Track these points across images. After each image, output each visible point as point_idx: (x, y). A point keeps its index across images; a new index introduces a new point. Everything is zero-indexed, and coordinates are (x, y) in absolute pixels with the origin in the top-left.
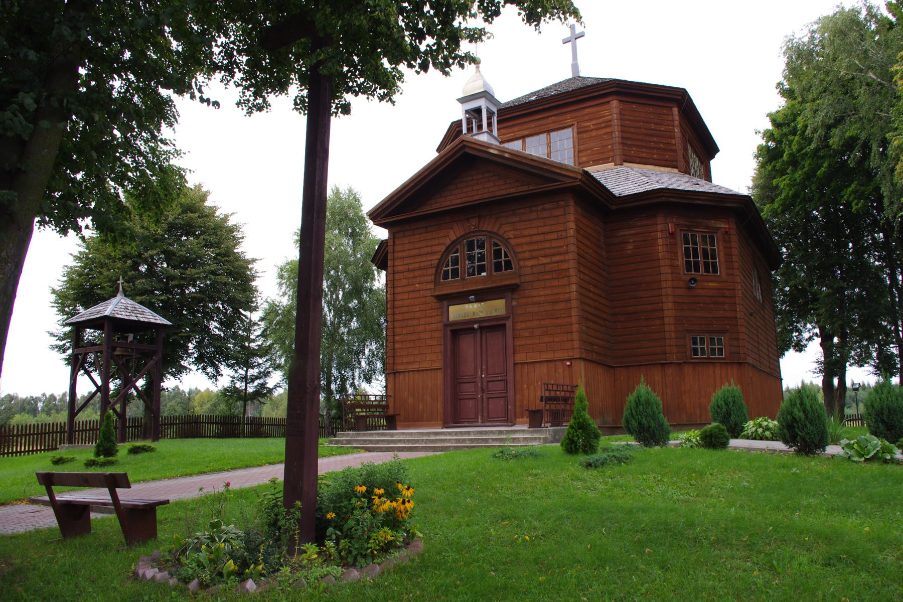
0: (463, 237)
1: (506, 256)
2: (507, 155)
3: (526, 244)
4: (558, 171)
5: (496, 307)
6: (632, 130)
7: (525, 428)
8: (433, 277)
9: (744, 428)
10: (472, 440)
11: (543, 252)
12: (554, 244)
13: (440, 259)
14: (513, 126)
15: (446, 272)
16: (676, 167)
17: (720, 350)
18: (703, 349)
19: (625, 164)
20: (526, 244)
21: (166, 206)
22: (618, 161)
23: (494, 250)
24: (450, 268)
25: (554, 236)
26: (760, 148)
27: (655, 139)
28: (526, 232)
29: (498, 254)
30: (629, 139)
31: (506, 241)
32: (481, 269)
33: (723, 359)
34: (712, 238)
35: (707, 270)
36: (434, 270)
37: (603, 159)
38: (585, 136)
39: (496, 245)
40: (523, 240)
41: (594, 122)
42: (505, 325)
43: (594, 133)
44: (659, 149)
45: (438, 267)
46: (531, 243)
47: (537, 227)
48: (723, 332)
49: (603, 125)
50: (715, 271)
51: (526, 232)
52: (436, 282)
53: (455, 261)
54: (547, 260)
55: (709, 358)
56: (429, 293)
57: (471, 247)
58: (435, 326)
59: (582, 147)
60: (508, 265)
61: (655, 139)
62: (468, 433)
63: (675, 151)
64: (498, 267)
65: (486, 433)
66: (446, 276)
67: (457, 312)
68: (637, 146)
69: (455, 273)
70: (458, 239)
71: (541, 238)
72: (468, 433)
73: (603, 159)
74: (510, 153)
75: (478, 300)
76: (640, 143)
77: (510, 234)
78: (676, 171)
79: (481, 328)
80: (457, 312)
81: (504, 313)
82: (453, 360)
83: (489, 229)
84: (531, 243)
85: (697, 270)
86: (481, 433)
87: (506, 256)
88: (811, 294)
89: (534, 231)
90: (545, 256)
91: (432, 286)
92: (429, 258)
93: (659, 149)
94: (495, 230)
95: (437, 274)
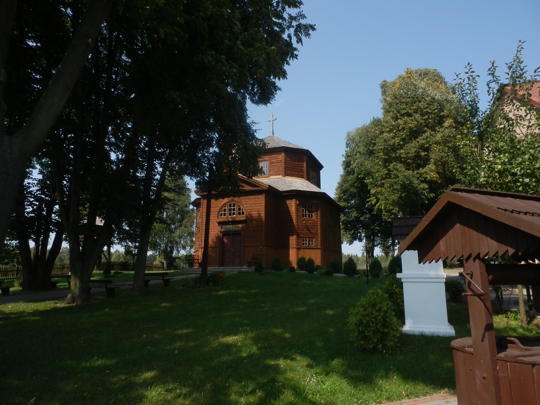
0: (228, 202)
1: (242, 210)
3: (249, 207)
4: (261, 184)
6: (289, 164)
7: (246, 267)
10: (229, 271)
11: (254, 210)
12: (259, 207)
13: (220, 209)
15: (222, 214)
16: (303, 178)
17: (312, 244)
18: (306, 243)
19: (286, 177)
20: (249, 207)
22: (283, 176)
24: (223, 212)
25: (258, 205)
26: (344, 162)
27: (297, 168)
28: (249, 203)
29: (240, 209)
30: (288, 167)
31: (242, 205)
32: (234, 214)
33: (314, 247)
34: (312, 206)
35: (309, 217)
36: (217, 213)
37: (278, 174)
38: (272, 165)
39: (239, 206)
41: (276, 160)
43: (276, 164)
44: (298, 171)
45: (219, 212)
46: (251, 206)
47: (253, 201)
48: (313, 238)
49: (279, 161)
50: (312, 217)
51: (249, 203)
52: (218, 217)
53: (225, 210)
55: (308, 246)
56: (215, 221)
57: (230, 206)
58: (213, 230)
59: (271, 169)
61: (297, 168)
62: (228, 269)
63: (303, 172)
65: (234, 269)
66: (221, 215)
68: (291, 170)
70: (226, 203)
71: (254, 205)
72: (228, 269)
73: (278, 174)
75: (232, 224)
76: (291, 169)
77: (244, 203)
78: (304, 179)
83: (237, 200)
84: (251, 206)
85: (306, 216)
86: (232, 269)
88: (466, 167)
89: (252, 203)
91: (216, 218)
92: (215, 208)
93: (298, 171)
94: (239, 201)
95: (218, 214)
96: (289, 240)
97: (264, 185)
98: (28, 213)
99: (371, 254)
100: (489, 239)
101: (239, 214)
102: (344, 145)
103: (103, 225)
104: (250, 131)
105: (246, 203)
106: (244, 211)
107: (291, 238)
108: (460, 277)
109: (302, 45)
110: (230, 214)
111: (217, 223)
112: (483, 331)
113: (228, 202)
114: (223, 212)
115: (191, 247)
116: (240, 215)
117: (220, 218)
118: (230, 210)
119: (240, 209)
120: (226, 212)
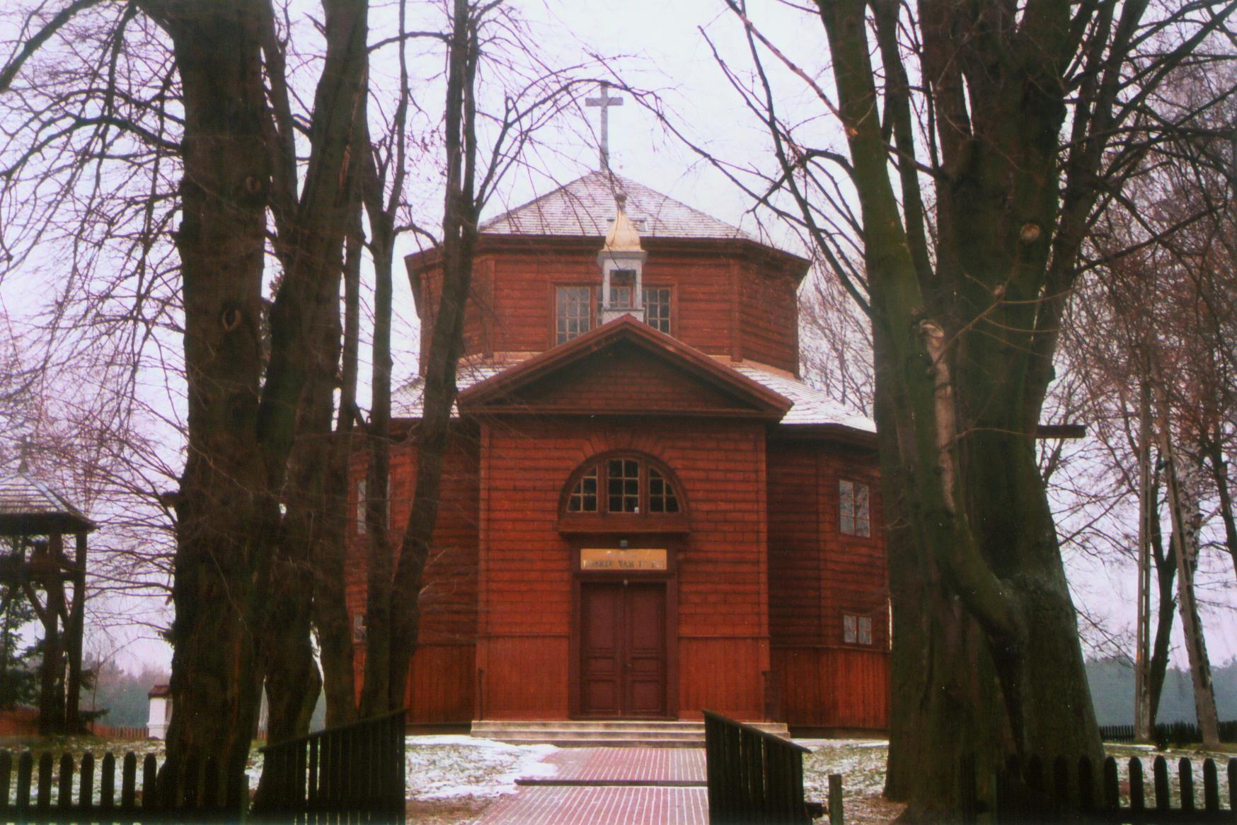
1: (669, 491)
2: (688, 357)
5: (653, 559)
8: (556, 505)
9: (1111, 305)
14: (653, 336)
21: (1122, 245)
23: (611, 499)
24: (581, 495)
29: (656, 486)
31: (671, 473)
36: (556, 496)
39: (654, 473)
40: (694, 474)
42: (664, 585)
45: (566, 489)
52: (560, 511)
54: (731, 506)
57: (616, 467)
60: (672, 505)
64: (656, 505)
67: (591, 559)
69: (590, 504)
74: (694, 357)
77: (678, 464)
79: (630, 585)
80: (591, 559)
81: (665, 568)
82: (582, 626)
87: (669, 491)
90: (726, 501)
91: (555, 518)
95: (562, 502)
98: (1126, 803)
99: (279, 119)
100: (1169, 648)
101: (656, 505)
104: (12, 650)
106: (675, 494)
108: (139, 725)
109: (699, 27)
110: (615, 505)
112: (600, 79)
114: (581, 495)
116: (619, 509)
118: (615, 487)
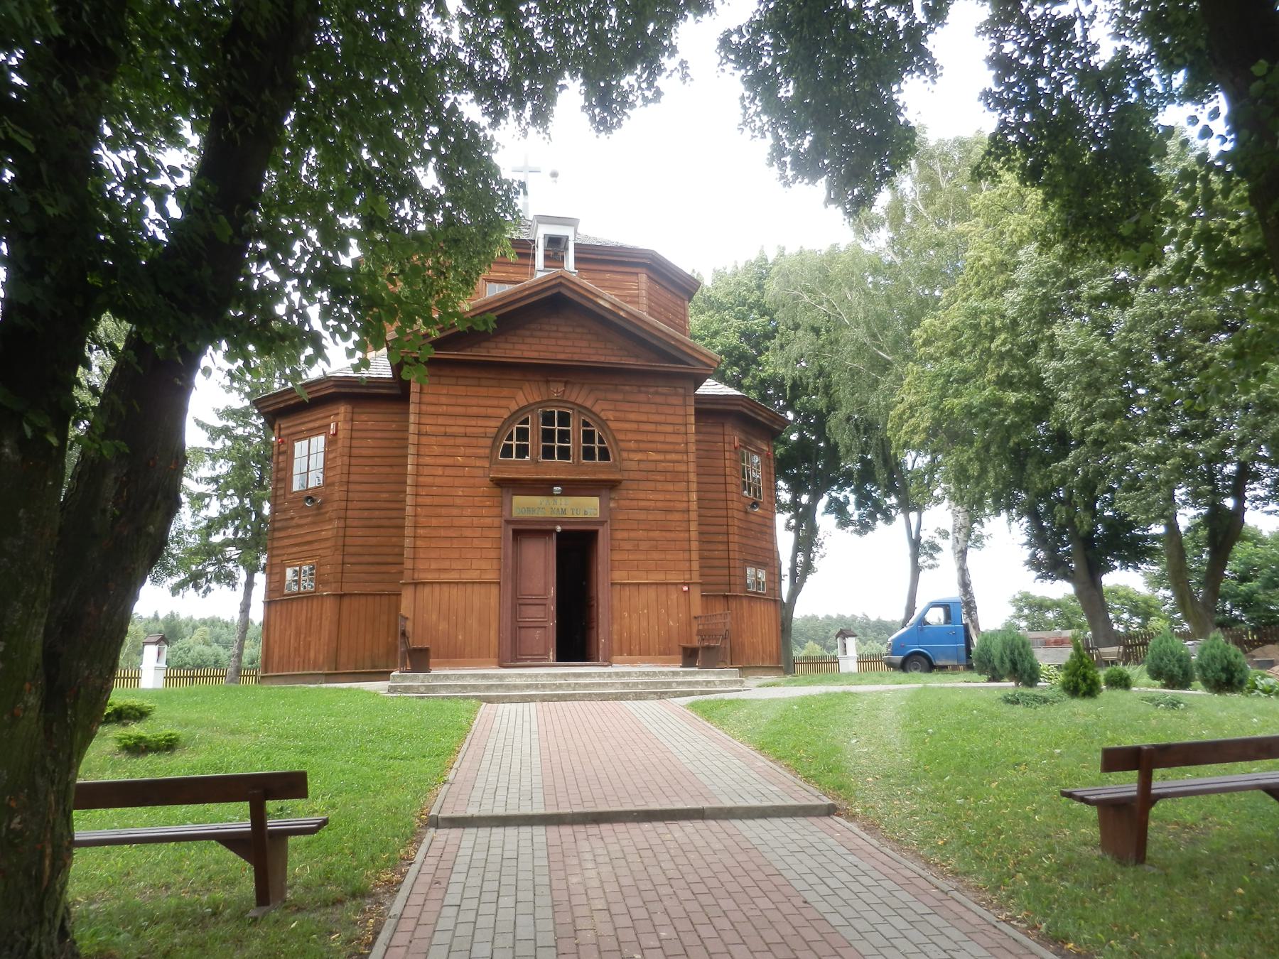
4: (689, 351)
29: (589, 436)
36: (489, 442)
39: (586, 424)
45: (496, 438)
51: (632, 416)
56: (480, 472)
57: (548, 419)
66: (507, 451)
71: (651, 427)
95: (493, 447)
96: (491, 827)
97: (701, 358)
102: (812, 247)
103: (1135, 793)
105: (618, 414)
107: (297, 445)
111: (1092, 812)
113: (539, 402)
115: (146, 78)
116: (553, 458)
117: (501, 463)
118: (548, 436)
119: (589, 436)
120: (529, 443)
